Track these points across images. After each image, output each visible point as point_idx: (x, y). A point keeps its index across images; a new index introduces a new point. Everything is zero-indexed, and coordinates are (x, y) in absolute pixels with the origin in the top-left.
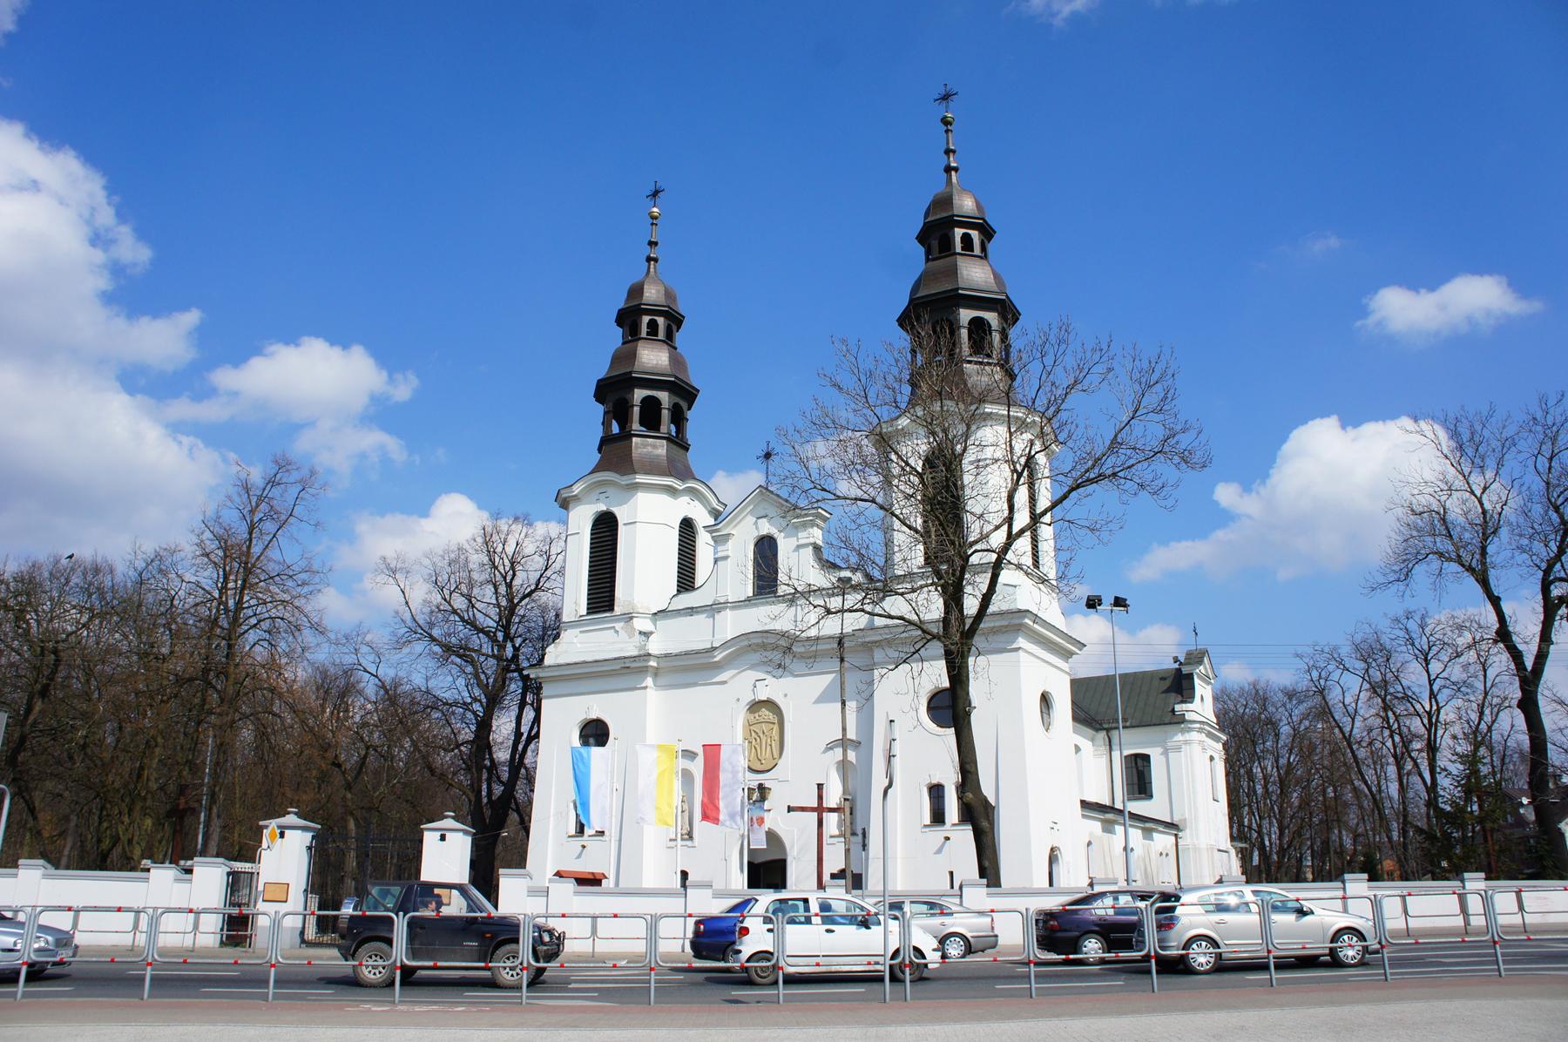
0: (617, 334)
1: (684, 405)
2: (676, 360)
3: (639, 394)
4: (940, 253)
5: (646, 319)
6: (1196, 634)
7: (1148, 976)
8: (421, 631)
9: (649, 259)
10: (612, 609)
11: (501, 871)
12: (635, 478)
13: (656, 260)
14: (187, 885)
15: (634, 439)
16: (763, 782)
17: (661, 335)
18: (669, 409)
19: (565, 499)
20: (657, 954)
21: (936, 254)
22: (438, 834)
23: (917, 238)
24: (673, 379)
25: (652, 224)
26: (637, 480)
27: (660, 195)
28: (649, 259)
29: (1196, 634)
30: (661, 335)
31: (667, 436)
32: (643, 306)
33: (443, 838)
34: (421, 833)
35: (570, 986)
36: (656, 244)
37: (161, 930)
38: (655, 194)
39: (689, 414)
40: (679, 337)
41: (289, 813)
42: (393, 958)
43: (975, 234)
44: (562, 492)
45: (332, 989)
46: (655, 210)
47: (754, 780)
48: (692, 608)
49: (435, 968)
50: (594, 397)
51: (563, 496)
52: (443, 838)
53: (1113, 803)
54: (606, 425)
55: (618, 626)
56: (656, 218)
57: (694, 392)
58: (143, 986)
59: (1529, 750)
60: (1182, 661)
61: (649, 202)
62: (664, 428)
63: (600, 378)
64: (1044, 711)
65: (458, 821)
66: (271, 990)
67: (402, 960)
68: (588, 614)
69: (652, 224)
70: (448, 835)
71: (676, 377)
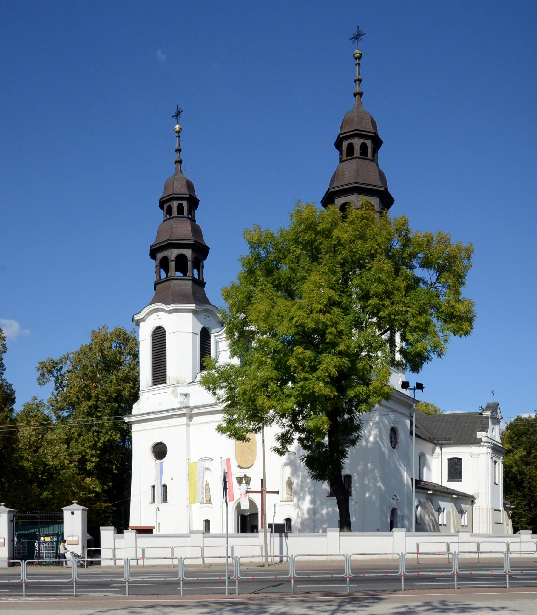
2: (196, 231)
4: (347, 157)
6: (493, 394)
7: (78, 573)
10: (166, 383)
11: (101, 528)
13: (361, 94)
14: (324, 539)
16: (245, 474)
19: (137, 320)
21: (345, 157)
22: (70, 512)
24: (193, 242)
27: (181, 115)
29: (493, 394)
33: (73, 513)
34: (62, 511)
35: (112, 585)
37: (136, 564)
38: (177, 115)
40: (198, 214)
41: (73, 503)
43: (369, 143)
44: (135, 317)
45: (8, 589)
46: (177, 126)
50: (150, 256)
51: (136, 319)
52: (73, 513)
53: (442, 483)
54: (158, 273)
58: (401, 582)
59: (306, 451)
60: (484, 408)
61: (174, 120)
62: (189, 274)
63: (151, 245)
64: (392, 437)
65: (80, 505)
66: (456, 583)
68: (154, 385)
70: (75, 512)
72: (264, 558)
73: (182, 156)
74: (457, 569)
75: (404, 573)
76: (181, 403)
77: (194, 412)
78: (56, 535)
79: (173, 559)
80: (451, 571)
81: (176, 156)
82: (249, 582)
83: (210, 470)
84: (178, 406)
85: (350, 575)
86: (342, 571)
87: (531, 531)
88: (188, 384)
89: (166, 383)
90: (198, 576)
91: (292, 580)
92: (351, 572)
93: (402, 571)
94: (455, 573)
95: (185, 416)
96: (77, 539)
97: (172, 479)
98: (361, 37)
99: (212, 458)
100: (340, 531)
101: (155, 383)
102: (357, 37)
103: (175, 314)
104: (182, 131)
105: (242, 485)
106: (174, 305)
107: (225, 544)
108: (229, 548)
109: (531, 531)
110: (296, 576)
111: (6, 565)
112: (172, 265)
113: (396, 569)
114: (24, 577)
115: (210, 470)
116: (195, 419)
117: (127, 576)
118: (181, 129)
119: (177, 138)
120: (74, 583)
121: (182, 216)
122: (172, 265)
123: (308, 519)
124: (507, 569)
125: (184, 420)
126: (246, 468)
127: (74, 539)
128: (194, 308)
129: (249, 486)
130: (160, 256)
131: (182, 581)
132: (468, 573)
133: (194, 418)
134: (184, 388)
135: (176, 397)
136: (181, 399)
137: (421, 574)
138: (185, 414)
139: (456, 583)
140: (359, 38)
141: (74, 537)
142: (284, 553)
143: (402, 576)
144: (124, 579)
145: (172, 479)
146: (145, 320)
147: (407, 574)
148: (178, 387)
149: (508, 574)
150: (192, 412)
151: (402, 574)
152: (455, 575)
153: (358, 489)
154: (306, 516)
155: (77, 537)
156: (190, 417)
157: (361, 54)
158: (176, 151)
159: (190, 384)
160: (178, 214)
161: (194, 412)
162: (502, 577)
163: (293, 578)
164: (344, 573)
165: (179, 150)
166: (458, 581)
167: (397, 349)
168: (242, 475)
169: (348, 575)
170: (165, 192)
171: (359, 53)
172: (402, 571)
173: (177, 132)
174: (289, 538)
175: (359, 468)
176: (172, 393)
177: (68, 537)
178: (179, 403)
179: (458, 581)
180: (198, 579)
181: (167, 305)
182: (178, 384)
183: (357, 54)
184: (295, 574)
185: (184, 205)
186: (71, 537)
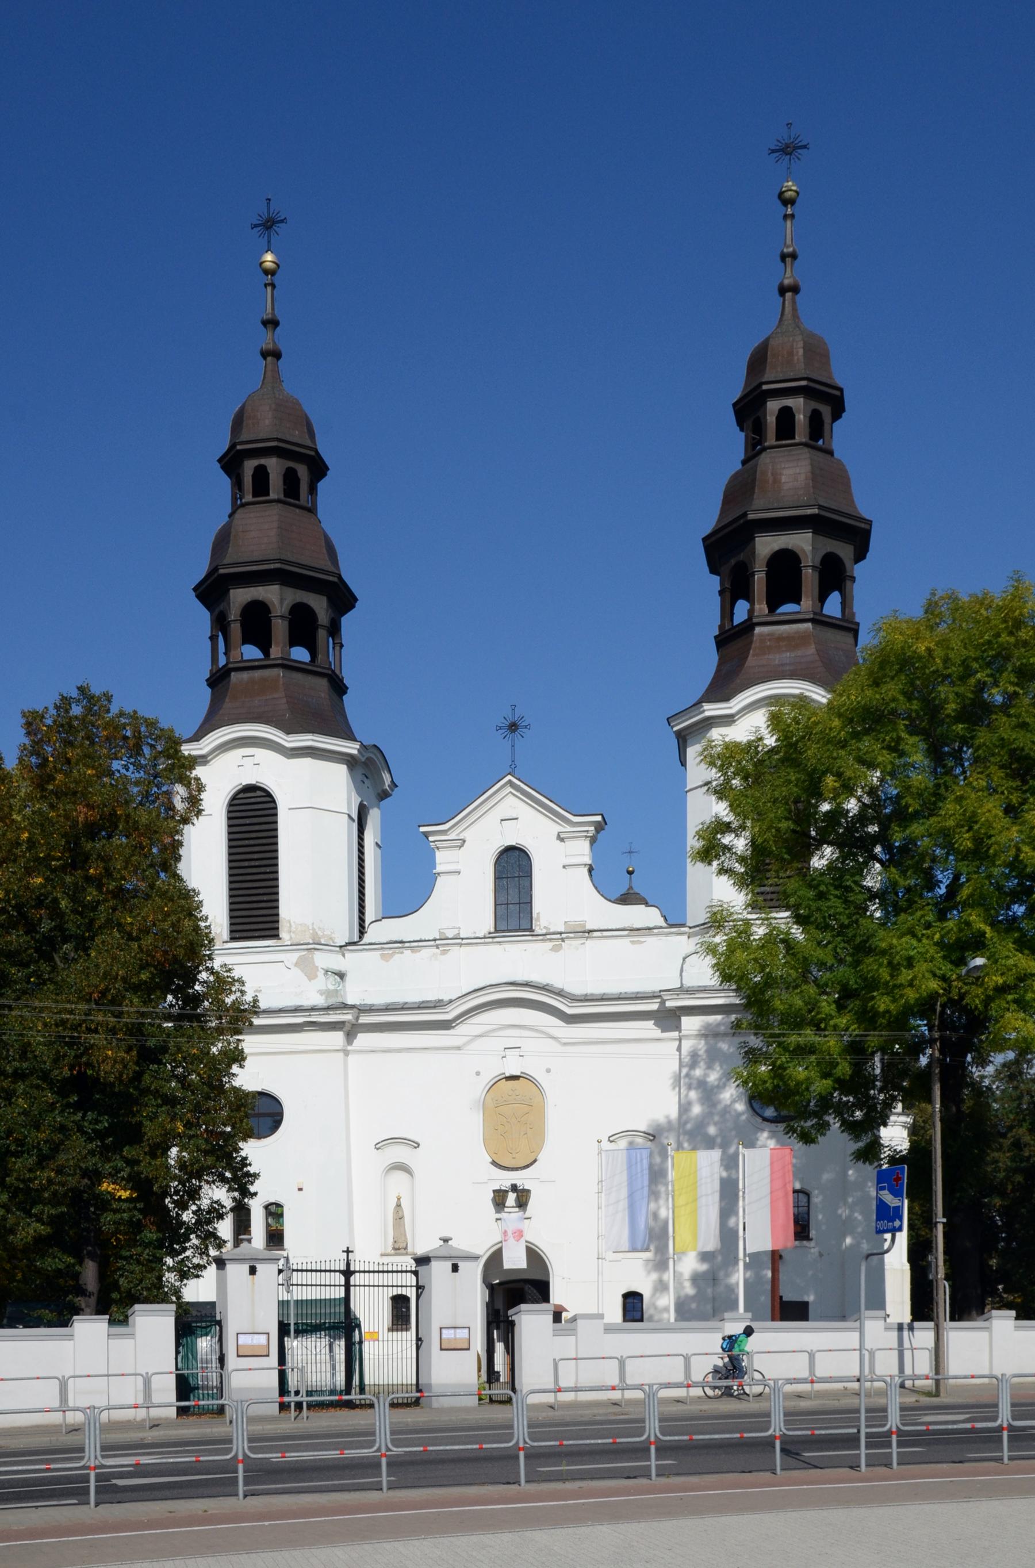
0: (737, 441)
1: (845, 551)
3: (766, 545)
5: (773, 406)
8: (722, 982)
9: (783, 290)
10: (276, 936)
12: (704, 711)
13: (795, 289)
15: (758, 630)
16: (514, 1182)
17: (801, 434)
18: (813, 567)
20: (525, 1406)
23: (219, 461)
24: (816, 511)
25: (785, 217)
26: (707, 714)
27: (281, 228)
28: (783, 290)
30: (801, 434)
31: (812, 616)
32: (765, 387)
33: (455, 1268)
36: (794, 256)
38: (269, 224)
39: (859, 570)
42: (377, 1445)
46: (269, 257)
47: (505, 1180)
48: (401, 942)
49: (48, 1470)
52: (455, 1268)
55: (292, 957)
56: (792, 202)
57: (863, 525)
67: (656, 1435)
68: (233, 939)
69: (785, 217)
70: (259, 1267)
71: (820, 507)
72: (856, 1385)
73: (282, 338)
74: (782, 1424)
75: (245, 1454)
76: (328, 993)
77: (364, 1019)
78: (342, 1327)
79: (64, 1411)
80: (82, 1458)
81: (266, 339)
82: (412, 1463)
83: (412, 1176)
84: (320, 1001)
85: (525, 1442)
86: (991, 1408)
87: (1013, 1313)
88: (341, 947)
89: (276, 936)
90: (560, 1436)
91: (653, 1448)
92: (392, 1440)
93: (653, 1429)
94: (383, 1451)
95: (340, 1029)
96: (467, 1336)
97: (300, 1189)
98: (799, 151)
99: (416, 1140)
100: (1017, 1318)
101: (237, 935)
102: (788, 150)
103: (308, 761)
104: (279, 272)
105: (506, 1210)
106: (310, 736)
107: (896, 1346)
108: (866, 1354)
109: (1013, 1313)
110: (661, 1437)
111: (172, 1412)
112: (280, 629)
113: (637, 1425)
114: (383, 1439)
115: (412, 1176)
116: (363, 1040)
117: (92, 1457)
118: (278, 265)
119: (269, 289)
120: (241, 1466)
121: (297, 502)
122: (280, 629)
123: (693, 1298)
124: (1004, 1416)
125: (337, 1038)
126: (516, 1169)
127: (458, 1336)
128: (355, 752)
129: (525, 1211)
130: (240, 597)
131: (242, 1461)
132: (334, 1454)
133: (360, 1035)
134: (329, 955)
135: (311, 976)
136: (323, 983)
137: (817, 1432)
138: (343, 1023)
139: (653, 1462)
140: (790, 154)
141: (458, 1331)
142: (908, 1371)
143: (651, 1443)
144: (375, 1448)
145: (300, 1189)
146: (208, 762)
147: (791, 1433)
148: (317, 953)
149: (386, 1456)
150: (360, 1021)
151: (652, 1439)
152: (382, 1455)
153: (824, 1228)
154: (689, 1290)
155: (265, 1336)
156: (351, 1031)
157: (797, 192)
158: (265, 323)
159: (349, 948)
160: (287, 494)
161: (364, 1019)
162: (371, 1466)
163: (654, 1443)
164: (230, 1450)
165: (271, 323)
166: (867, 1447)
167: (811, 903)
168: (506, 1185)
169: (383, 1451)
170: (756, 466)
171: (795, 191)
172: (653, 1429)
173: (266, 272)
174: (916, 1333)
175: (826, 1177)
176: (296, 965)
177: (444, 1331)
178: (321, 992)
179: (900, 1444)
180: (561, 1445)
181: (288, 733)
182: (316, 945)
183: (790, 193)
184: (247, 1451)
185: (299, 474)
186: (452, 1331)
